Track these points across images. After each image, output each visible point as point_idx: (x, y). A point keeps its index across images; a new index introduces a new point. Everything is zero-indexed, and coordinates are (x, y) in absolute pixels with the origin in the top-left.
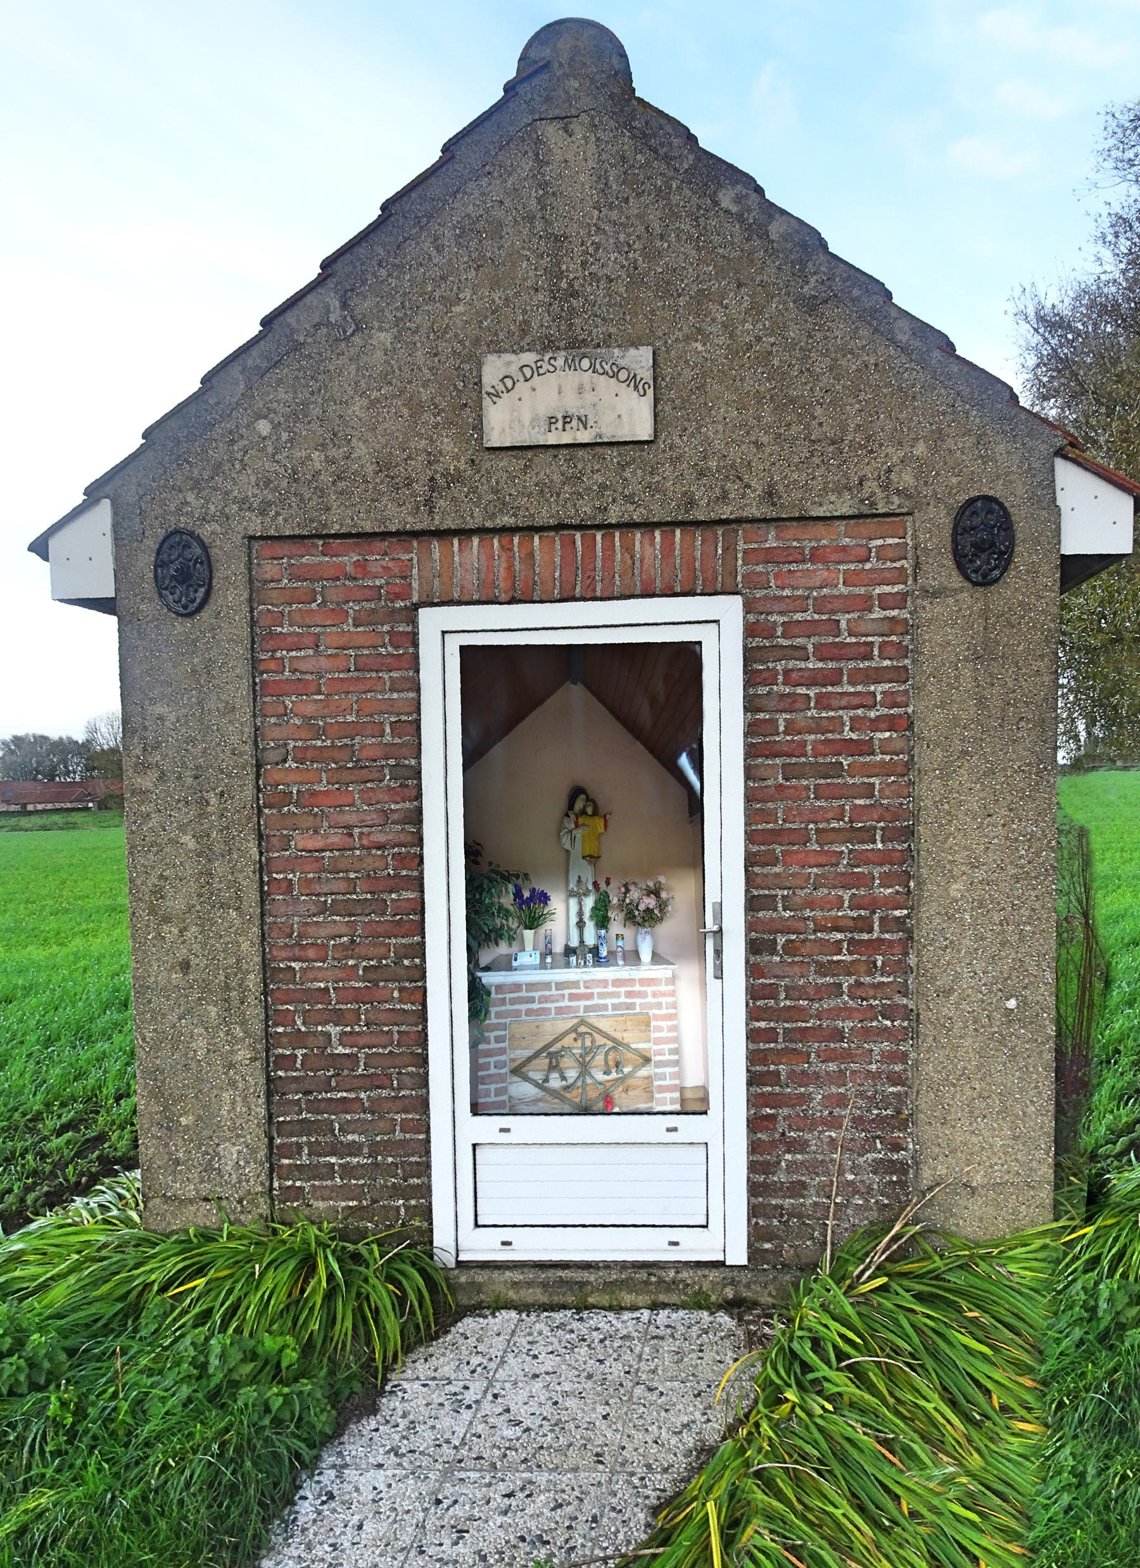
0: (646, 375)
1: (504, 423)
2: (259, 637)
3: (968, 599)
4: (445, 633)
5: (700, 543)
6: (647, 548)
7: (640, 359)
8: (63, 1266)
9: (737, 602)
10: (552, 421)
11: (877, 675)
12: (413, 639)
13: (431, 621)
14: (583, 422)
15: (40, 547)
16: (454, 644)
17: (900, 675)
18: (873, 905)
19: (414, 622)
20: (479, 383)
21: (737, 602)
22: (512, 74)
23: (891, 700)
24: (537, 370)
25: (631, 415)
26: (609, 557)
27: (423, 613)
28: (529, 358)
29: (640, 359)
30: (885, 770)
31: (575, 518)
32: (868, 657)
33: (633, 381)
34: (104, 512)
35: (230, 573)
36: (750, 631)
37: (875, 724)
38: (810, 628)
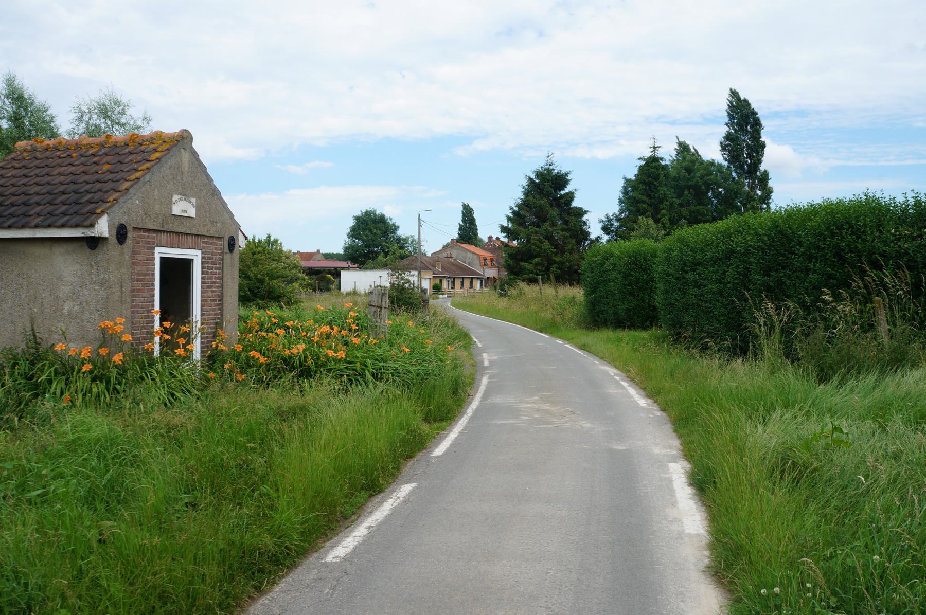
1: (176, 210)
6: (190, 240)
13: (199, 253)
25: (192, 213)
35: (130, 235)
36: (203, 258)
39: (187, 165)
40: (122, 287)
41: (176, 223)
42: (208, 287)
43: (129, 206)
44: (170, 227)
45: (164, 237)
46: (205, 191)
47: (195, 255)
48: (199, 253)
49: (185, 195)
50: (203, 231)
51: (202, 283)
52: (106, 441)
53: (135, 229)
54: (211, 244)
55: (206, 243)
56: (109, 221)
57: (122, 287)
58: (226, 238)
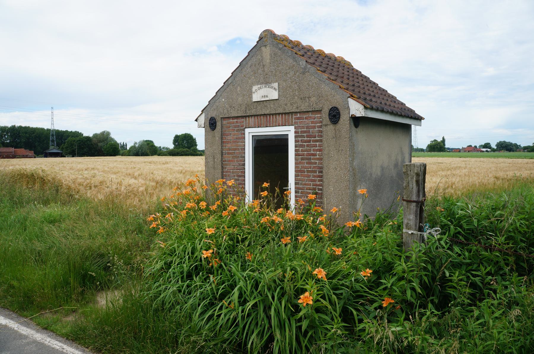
0: (277, 88)
1: (256, 97)
2: (222, 135)
3: (331, 127)
4: (250, 133)
5: (285, 116)
6: (279, 118)
7: (276, 85)
8: (24, 330)
9: (293, 127)
10: (262, 96)
11: (317, 141)
12: (244, 134)
13: (247, 131)
14: (267, 96)
15: (196, 120)
16: (251, 135)
17: (321, 141)
18: (316, 185)
19: (244, 131)
20: (279, 92)
21: (293, 127)
22: (258, 40)
23: (320, 146)
24: (260, 88)
25: (274, 95)
26: (273, 119)
27: (246, 130)
28: (259, 86)
29: (276, 85)
30: (318, 159)
31: (265, 114)
32: (315, 137)
33: (275, 89)
34: (203, 115)
35: (219, 124)
36: (295, 132)
37: (317, 150)
38: (305, 132)
39: (269, 57)
40: (214, 158)
41: (259, 108)
42: (302, 159)
43: (217, 104)
44: (253, 112)
45: (252, 120)
46: (292, 73)
47: (250, 133)
48: (247, 131)
49: (266, 82)
50: (289, 109)
51: (296, 155)
52: (425, 269)
53: (223, 118)
54: (306, 118)
55: (298, 118)
56: (205, 116)
57: (214, 158)
58: (326, 110)
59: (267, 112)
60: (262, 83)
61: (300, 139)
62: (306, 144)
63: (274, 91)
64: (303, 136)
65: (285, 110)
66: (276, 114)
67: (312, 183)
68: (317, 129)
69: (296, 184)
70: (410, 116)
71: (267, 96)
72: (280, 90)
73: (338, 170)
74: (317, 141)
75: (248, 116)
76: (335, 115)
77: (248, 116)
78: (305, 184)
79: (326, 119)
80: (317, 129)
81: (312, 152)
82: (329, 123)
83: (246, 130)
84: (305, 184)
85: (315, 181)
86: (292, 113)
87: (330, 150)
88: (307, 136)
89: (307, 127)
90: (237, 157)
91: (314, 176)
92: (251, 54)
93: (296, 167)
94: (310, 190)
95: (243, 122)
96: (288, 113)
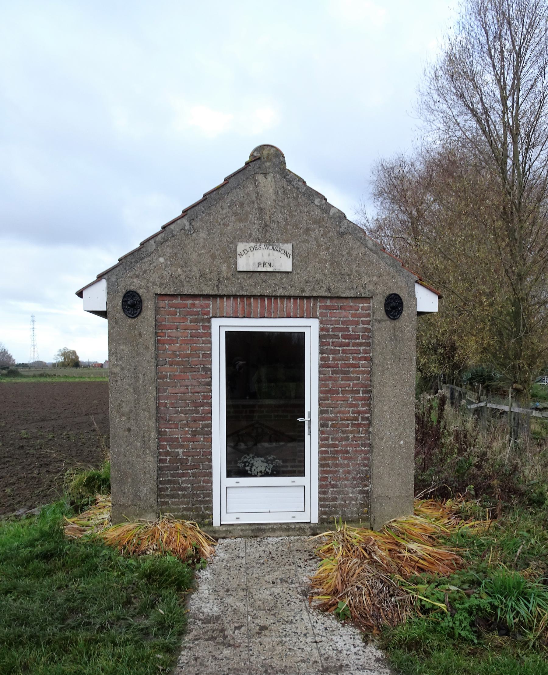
0: (290, 252)
1: (244, 263)
2: (158, 326)
3: (389, 323)
4: (220, 328)
5: (302, 301)
7: (289, 247)
10: (259, 264)
11: (361, 344)
12: (210, 328)
13: (216, 323)
15: (80, 294)
18: (359, 413)
19: (210, 322)
23: (365, 352)
25: (285, 264)
27: (213, 320)
28: (252, 244)
29: (289, 247)
31: (262, 294)
33: (286, 253)
35: (149, 305)
36: (321, 330)
37: (360, 359)
38: (340, 330)
42: (333, 372)
45: (228, 304)
48: (216, 323)
49: (266, 239)
54: (342, 308)
55: (327, 307)
56: (108, 288)
59: (268, 292)
60: (258, 241)
61: (331, 340)
62: (340, 349)
63: (284, 257)
64: (337, 337)
65: (303, 290)
66: (282, 297)
67: (351, 410)
68: (361, 326)
69: (321, 412)
70: (262, 274)
71: (269, 265)
72: (297, 257)
73: (398, 388)
74: (361, 344)
75: (221, 296)
76: (394, 306)
77: (221, 296)
78: (340, 412)
79: (381, 313)
80: (361, 326)
81: (351, 362)
82: (386, 318)
83: (213, 320)
84: (340, 412)
85: (356, 406)
86: (315, 298)
87: (385, 359)
88: (344, 337)
89: (344, 323)
90: (192, 369)
91: (354, 399)
92: (232, 182)
93: (320, 386)
94: (347, 420)
95: (208, 306)
96: (308, 298)
